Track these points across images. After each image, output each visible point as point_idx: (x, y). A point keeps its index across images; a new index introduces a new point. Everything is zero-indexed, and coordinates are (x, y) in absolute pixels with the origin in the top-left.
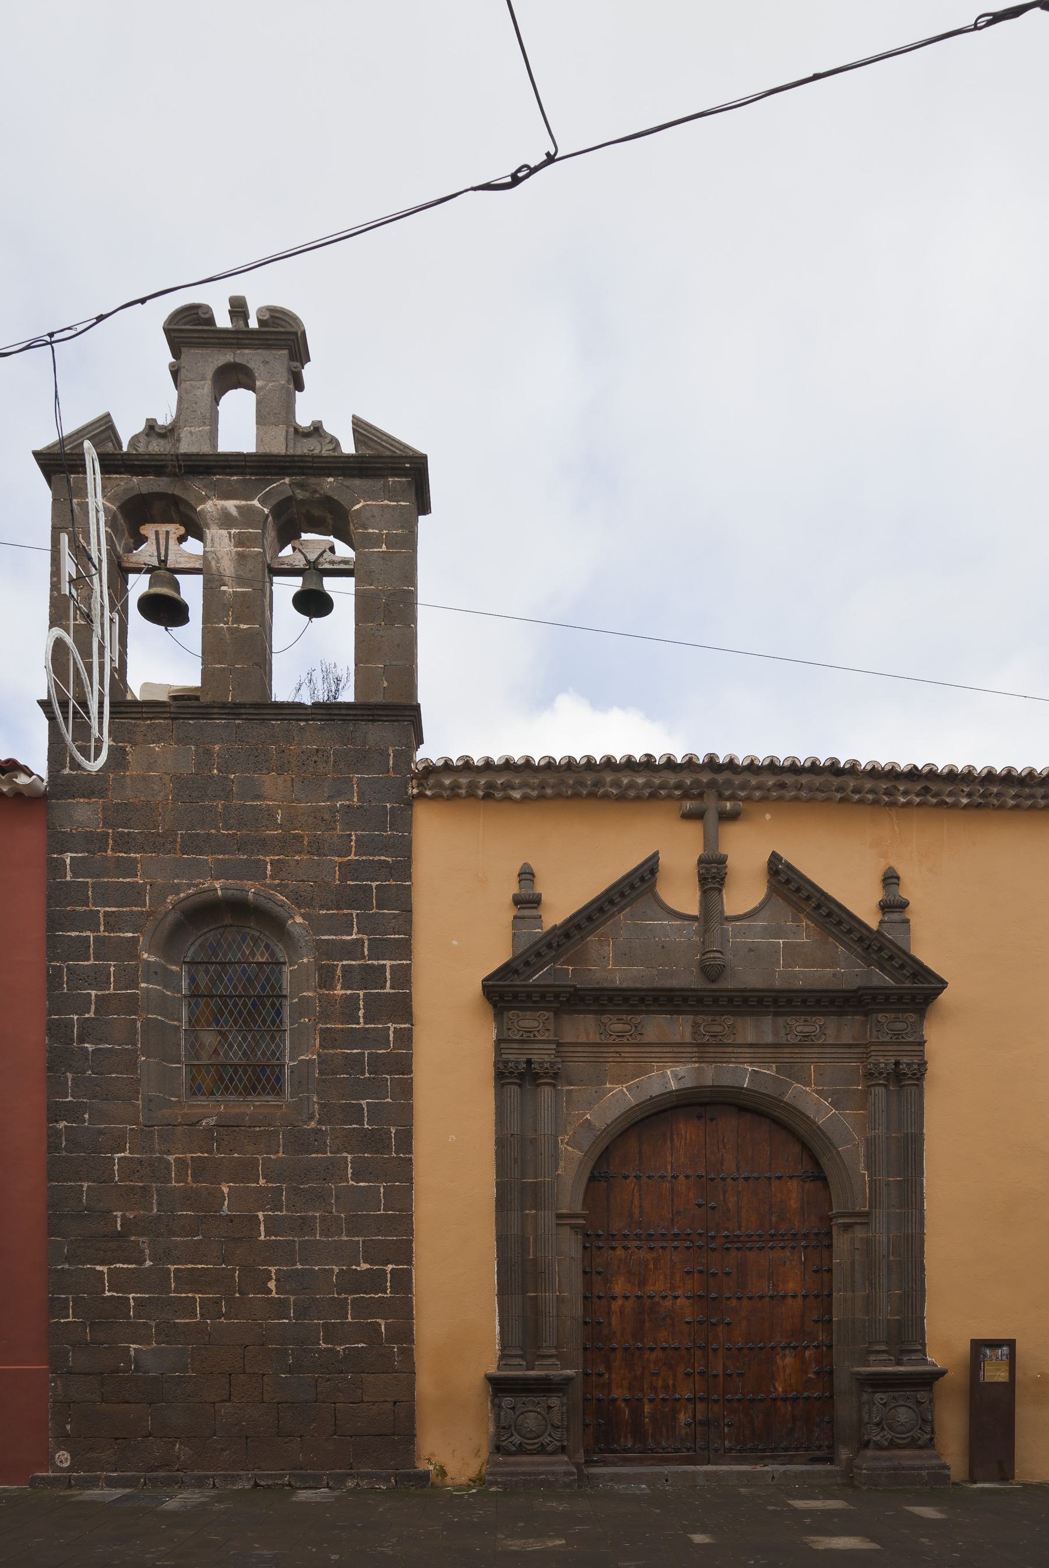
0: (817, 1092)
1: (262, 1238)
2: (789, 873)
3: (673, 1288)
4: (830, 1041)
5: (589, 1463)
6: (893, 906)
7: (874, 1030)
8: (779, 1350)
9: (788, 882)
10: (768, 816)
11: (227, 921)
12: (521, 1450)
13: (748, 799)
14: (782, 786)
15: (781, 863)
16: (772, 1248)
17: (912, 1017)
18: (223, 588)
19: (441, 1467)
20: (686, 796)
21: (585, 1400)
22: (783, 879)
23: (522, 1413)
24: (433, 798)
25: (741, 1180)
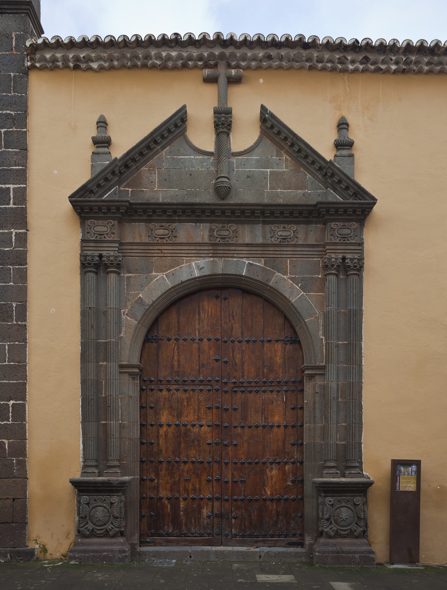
0: (291, 279)
2: (273, 120)
3: (199, 419)
4: (300, 242)
5: (142, 543)
6: (344, 145)
7: (329, 235)
8: (268, 464)
9: (272, 127)
10: (261, 81)
12: (93, 534)
13: (248, 68)
14: (269, 57)
15: (267, 114)
16: (264, 391)
17: (356, 225)
19: (44, 546)
20: (206, 66)
21: (142, 498)
22: (270, 125)
23: (94, 508)
24: (41, 69)
25: (244, 343)
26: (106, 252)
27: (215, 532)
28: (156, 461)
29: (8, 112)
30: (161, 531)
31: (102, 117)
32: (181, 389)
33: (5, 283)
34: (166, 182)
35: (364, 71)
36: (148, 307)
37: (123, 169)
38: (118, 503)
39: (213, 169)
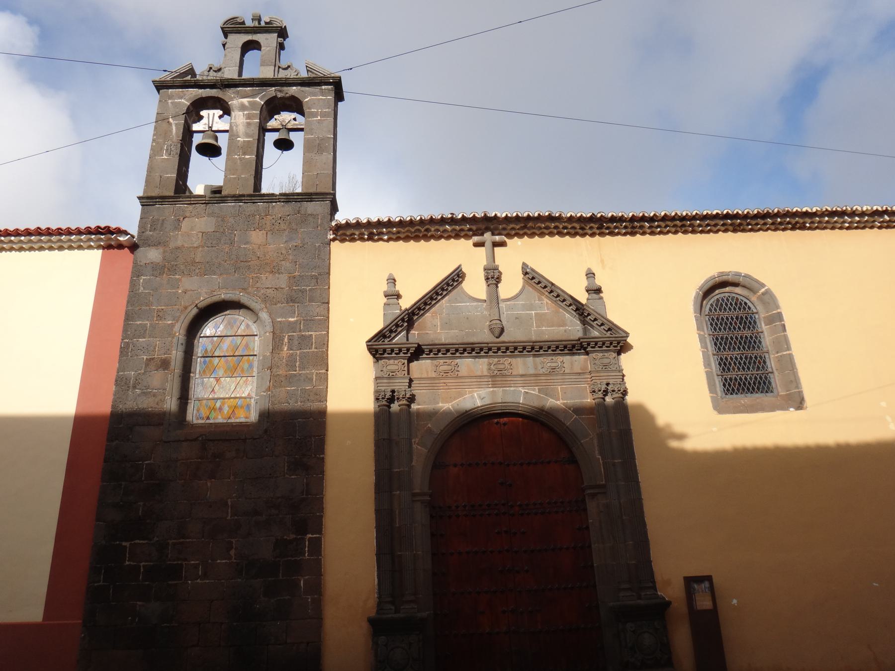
22: (531, 277)
31: (589, 269)
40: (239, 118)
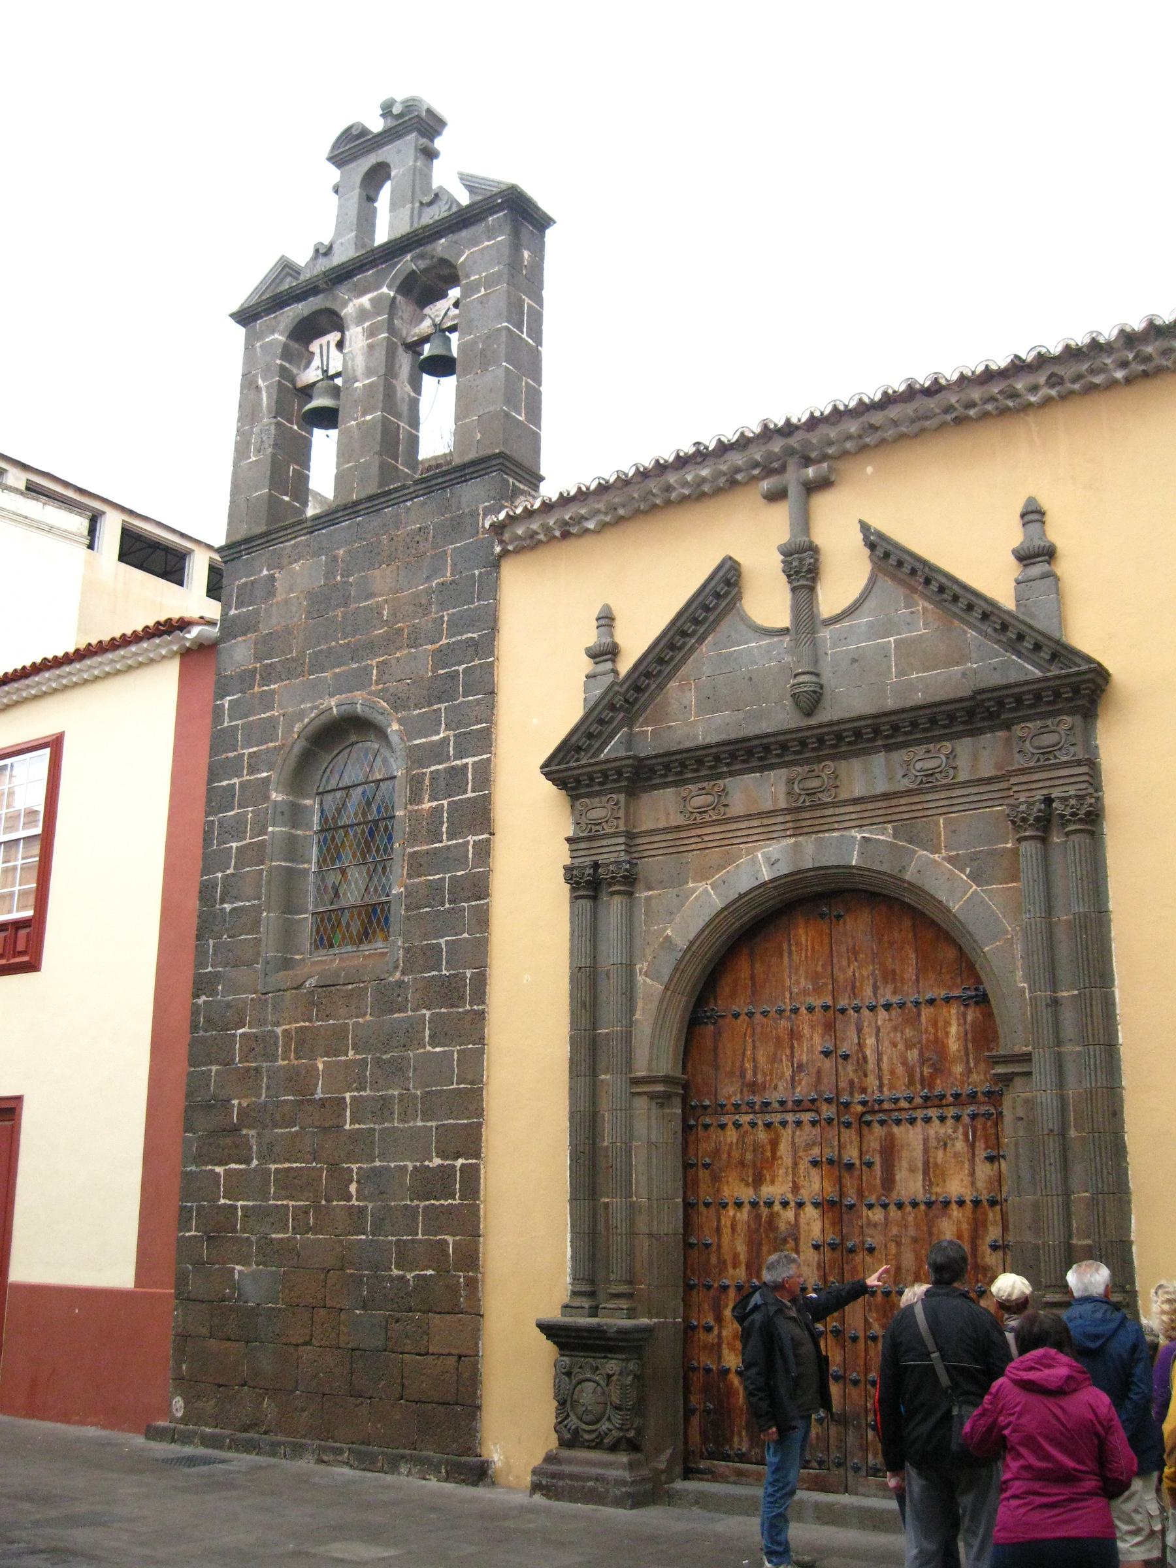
0: (950, 859)
1: (347, 1127)
4: (963, 776)
6: (1037, 556)
10: (869, 470)
11: (353, 739)
14: (874, 428)
15: (872, 534)
18: (356, 385)
20: (769, 472)
21: (688, 1370)
23: (579, 1383)
24: (518, 551)
26: (605, 856)
27: (832, 1457)
28: (716, 1285)
29: (470, 635)
30: (727, 1448)
31: (1031, 500)
32: (760, 1123)
33: (456, 934)
34: (710, 702)
35: (1063, 397)
36: (681, 954)
37: (632, 695)
38: (620, 1374)
39: (790, 659)
40: (356, 336)
